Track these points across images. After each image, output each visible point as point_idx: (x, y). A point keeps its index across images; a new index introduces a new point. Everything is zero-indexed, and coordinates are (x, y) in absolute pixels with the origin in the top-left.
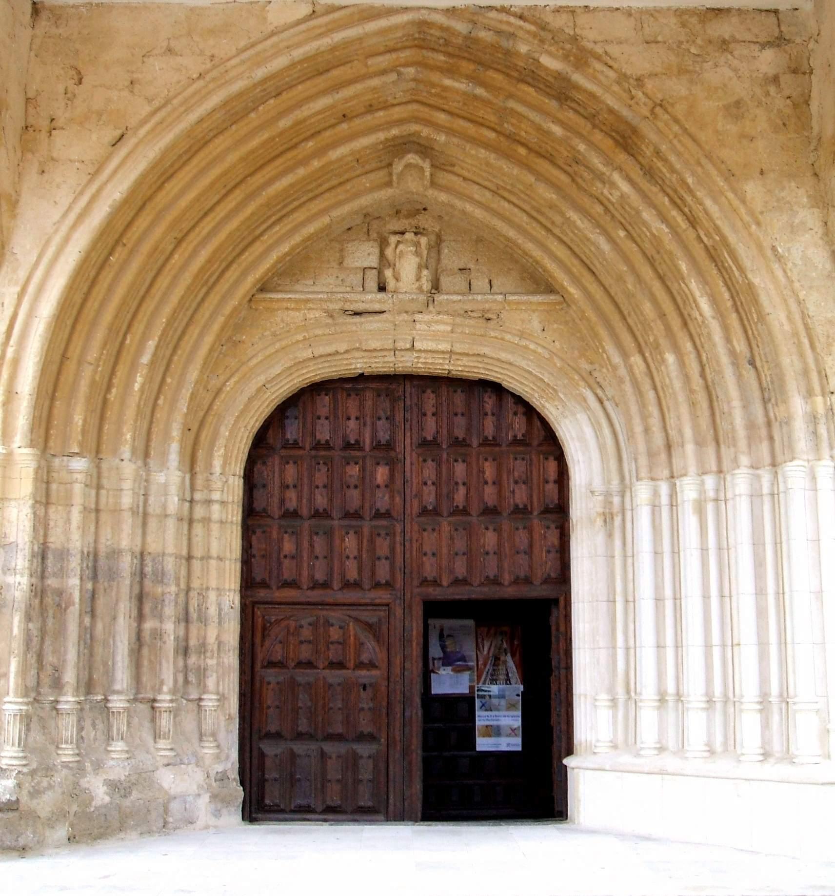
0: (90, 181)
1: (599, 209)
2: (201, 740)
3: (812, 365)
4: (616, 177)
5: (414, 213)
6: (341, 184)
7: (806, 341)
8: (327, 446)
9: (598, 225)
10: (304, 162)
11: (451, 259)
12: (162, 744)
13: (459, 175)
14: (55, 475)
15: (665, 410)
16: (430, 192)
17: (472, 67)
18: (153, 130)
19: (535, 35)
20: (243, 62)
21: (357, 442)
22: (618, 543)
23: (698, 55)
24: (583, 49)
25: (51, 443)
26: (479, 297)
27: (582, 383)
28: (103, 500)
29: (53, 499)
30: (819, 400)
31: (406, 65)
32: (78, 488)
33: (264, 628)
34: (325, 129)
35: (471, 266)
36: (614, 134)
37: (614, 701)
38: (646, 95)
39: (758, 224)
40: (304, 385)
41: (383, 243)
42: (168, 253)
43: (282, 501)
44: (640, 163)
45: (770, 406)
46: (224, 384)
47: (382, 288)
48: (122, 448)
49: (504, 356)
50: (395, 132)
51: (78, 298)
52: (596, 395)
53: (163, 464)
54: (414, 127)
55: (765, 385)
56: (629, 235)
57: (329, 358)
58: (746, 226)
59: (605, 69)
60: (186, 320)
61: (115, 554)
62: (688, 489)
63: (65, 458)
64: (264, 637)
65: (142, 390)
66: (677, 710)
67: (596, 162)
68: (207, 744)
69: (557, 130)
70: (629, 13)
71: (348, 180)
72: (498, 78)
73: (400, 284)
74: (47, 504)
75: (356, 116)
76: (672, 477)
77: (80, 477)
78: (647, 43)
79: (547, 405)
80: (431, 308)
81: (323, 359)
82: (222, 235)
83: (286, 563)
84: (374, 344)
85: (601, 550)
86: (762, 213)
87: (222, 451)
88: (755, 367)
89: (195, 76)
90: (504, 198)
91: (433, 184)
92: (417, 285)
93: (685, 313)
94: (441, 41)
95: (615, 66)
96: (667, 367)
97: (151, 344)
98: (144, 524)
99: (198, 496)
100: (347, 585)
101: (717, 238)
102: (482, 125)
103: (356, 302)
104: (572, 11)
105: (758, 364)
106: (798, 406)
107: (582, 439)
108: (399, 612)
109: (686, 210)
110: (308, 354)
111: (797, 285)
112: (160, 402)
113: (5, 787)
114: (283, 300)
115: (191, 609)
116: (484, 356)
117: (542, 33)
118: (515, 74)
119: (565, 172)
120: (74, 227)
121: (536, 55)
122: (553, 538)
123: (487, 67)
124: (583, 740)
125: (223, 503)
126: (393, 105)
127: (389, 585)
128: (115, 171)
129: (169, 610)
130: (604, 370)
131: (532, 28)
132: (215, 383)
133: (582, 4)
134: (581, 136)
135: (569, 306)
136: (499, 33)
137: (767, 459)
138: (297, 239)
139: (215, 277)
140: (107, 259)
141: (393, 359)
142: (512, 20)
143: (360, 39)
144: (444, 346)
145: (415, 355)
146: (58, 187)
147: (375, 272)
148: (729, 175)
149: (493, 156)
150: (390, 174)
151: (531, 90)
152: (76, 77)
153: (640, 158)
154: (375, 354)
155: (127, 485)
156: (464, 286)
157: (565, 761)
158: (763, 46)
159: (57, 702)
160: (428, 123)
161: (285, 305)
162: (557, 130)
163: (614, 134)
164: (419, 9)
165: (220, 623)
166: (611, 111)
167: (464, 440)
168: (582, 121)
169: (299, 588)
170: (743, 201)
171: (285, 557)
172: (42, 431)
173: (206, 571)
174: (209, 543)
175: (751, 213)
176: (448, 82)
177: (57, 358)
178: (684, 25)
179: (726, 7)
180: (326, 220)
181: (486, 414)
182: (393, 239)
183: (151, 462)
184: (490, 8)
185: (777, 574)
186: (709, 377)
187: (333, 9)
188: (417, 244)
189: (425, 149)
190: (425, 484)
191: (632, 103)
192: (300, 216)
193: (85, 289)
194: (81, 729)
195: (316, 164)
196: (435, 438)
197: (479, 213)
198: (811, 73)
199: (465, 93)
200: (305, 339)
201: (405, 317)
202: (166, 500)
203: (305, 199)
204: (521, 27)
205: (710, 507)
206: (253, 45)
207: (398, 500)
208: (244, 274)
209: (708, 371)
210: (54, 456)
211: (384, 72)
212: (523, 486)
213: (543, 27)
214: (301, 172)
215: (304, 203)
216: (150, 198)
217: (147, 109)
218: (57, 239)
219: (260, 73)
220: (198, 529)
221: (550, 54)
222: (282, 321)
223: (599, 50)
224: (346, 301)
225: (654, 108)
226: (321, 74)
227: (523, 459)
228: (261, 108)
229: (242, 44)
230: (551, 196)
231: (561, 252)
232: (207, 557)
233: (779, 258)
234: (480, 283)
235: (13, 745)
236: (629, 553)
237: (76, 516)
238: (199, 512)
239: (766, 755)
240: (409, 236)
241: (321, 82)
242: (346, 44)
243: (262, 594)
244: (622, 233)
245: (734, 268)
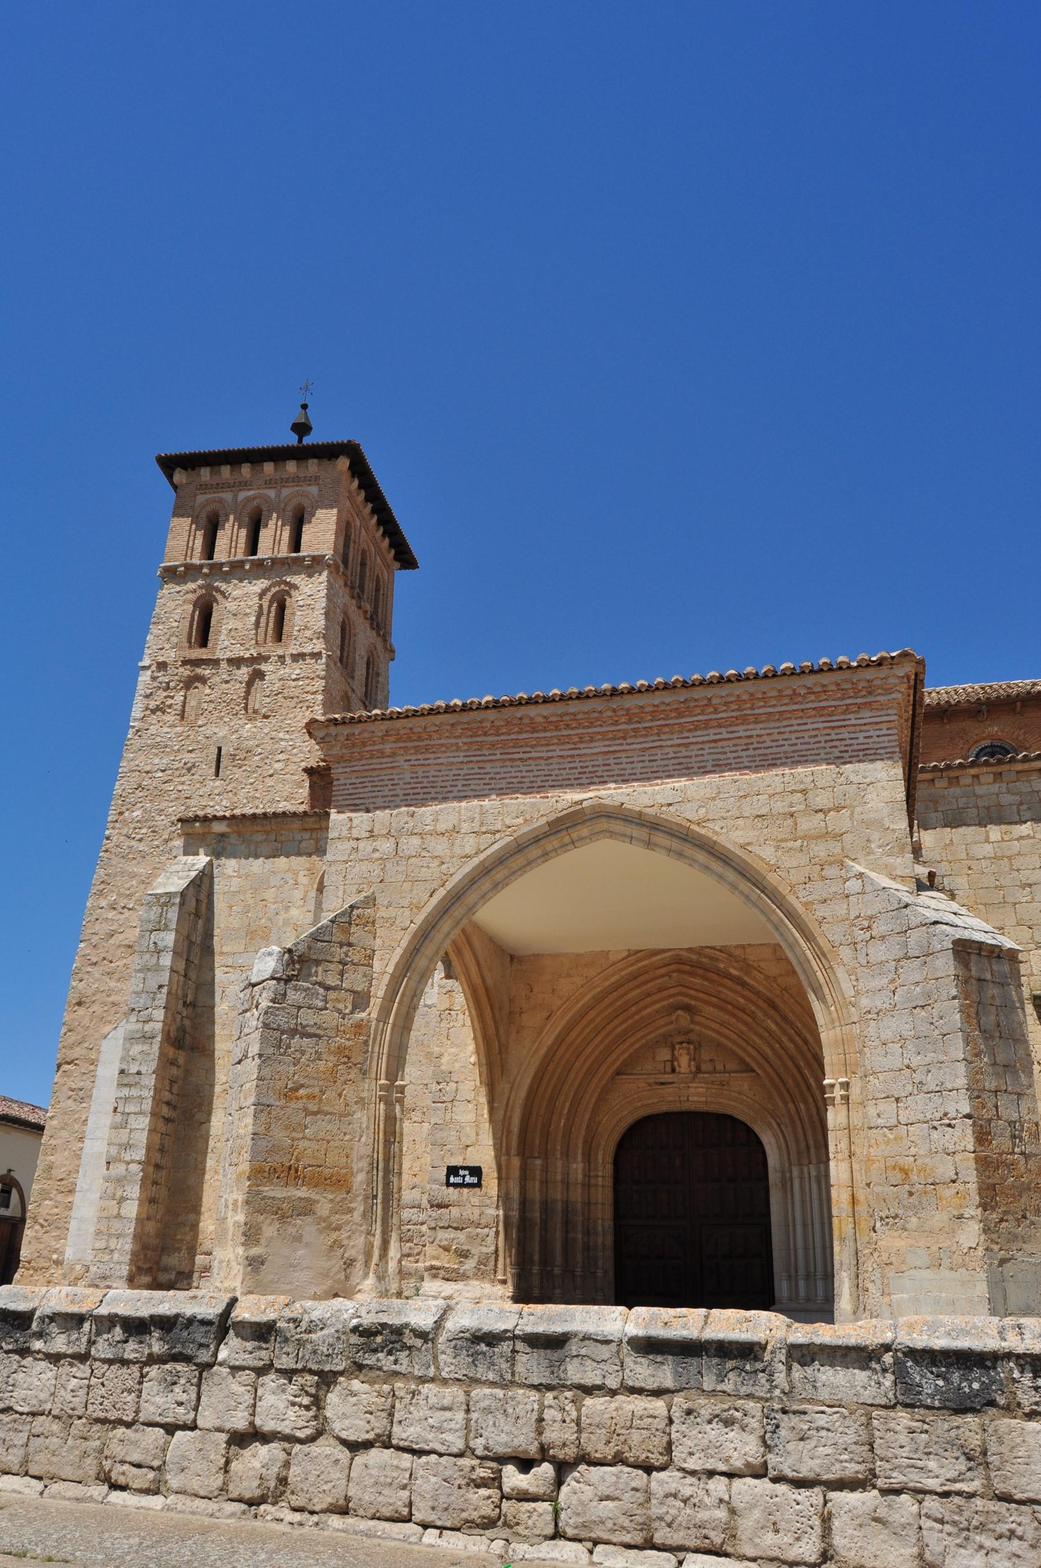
10: (631, 1017)
12: (578, 1292)
24: (749, 965)
31: (673, 972)
32: (538, 1172)
37: (790, 1276)
41: (673, 1049)
50: (671, 1000)
74: (525, 1180)
91: (692, 1021)
98: (568, 1188)
99: (592, 1174)
104: (743, 947)
125: (603, 1177)
129: (579, 1229)
144: (703, 1099)
168: (752, 995)
184: (707, 947)
188: (688, 1049)
192: (632, 1040)
194: (542, 1282)
195: (636, 1017)
214: (630, 1022)
217: (560, 1002)
219: (607, 983)
220: (593, 1189)
223: (755, 964)
229: (600, 970)
232: (596, 1203)
237: (537, 1184)
238: (593, 1181)
241: (635, 983)
242: (645, 966)
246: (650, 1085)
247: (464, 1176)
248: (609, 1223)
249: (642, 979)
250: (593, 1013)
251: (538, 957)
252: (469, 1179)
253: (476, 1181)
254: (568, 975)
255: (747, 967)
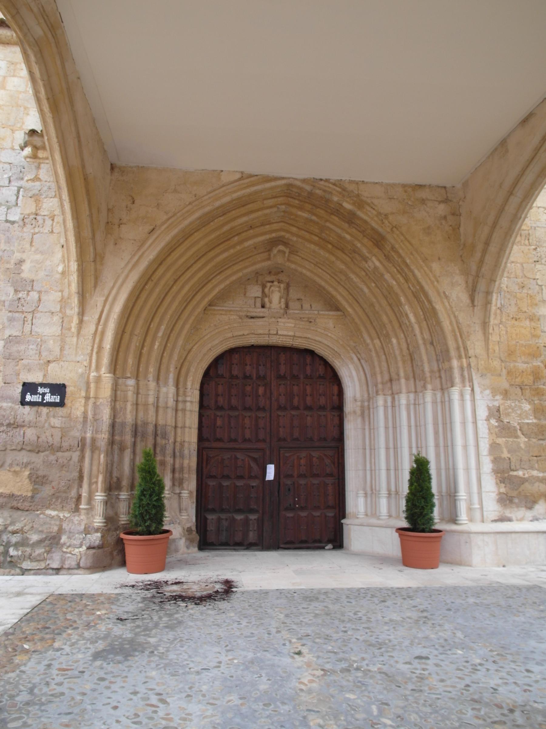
0: (139, 249)
1: (363, 273)
2: (180, 512)
3: (461, 345)
4: (374, 259)
5: (277, 274)
6: (247, 258)
7: (458, 334)
8: (237, 377)
9: (363, 281)
10: (233, 247)
11: (294, 294)
13: (300, 256)
14: (119, 387)
15: (390, 364)
16: (288, 264)
17: (310, 206)
18: (168, 227)
19: (340, 193)
20: (210, 198)
21: (250, 375)
22: (367, 423)
23: (412, 205)
25: (117, 372)
26: (307, 312)
27: (351, 352)
28: (140, 400)
29: (118, 398)
30: (464, 360)
33: (207, 460)
34: (243, 232)
35: (303, 298)
36: (372, 240)
37: (366, 494)
38: (389, 222)
39: (438, 281)
40: (227, 349)
41: (264, 286)
42: (171, 285)
43: (216, 402)
44: (383, 253)
45: (440, 363)
46: (192, 348)
47: (263, 307)
48: (149, 376)
49: (317, 338)
50: (274, 235)
51: (131, 305)
52: (357, 357)
53: (166, 384)
54: (283, 234)
55: (437, 353)
56: (377, 286)
57: (240, 337)
58: (432, 283)
59: (372, 210)
60: (177, 317)
61: (145, 424)
62: (403, 400)
63: (124, 379)
64: (207, 464)
65: (158, 348)
66: (396, 498)
67: (365, 251)
68: (183, 514)
69: (348, 237)
70: (381, 184)
71: (250, 257)
72: (322, 212)
73: (271, 305)
75: (257, 227)
76: (393, 394)
77: (131, 388)
78: (390, 199)
79: (335, 361)
80: (285, 316)
81: (237, 338)
82: (195, 279)
83: (218, 430)
84: (261, 332)
85: (360, 426)
86: (439, 277)
87: (191, 378)
88: (433, 345)
89: (187, 203)
90: (320, 268)
92: (279, 305)
93: (401, 321)
94: (297, 194)
95: (376, 208)
96: (392, 345)
97: (163, 327)
100: (245, 440)
101: (418, 287)
102: (312, 233)
103: (253, 312)
104: (357, 183)
105: (435, 344)
106: (455, 363)
107: (351, 377)
108: (268, 452)
109: (404, 274)
110: (230, 335)
111: (454, 309)
112: (165, 355)
113: (97, 536)
114: (220, 310)
115: (177, 451)
116: (309, 338)
117: (344, 192)
118: (329, 211)
119: (349, 257)
120: (131, 271)
121: (341, 202)
122: (336, 421)
123: (317, 207)
124: (352, 511)
125: (191, 402)
126: (273, 223)
127: (264, 441)
128: (152, 244)
130: (361, 346)
131: (340, 190)
132: (188, 347)
133: (362, 180)
134: (359, 240)
135: (346, 317)
136: (325, 191)
137: (439, 386)
138: (228, 282)
139: (190, 298)
140: (144, 287)
141: (268, 339)
142: (331, 185)
143: (262, 191)
144: (291, 333)
145: (278, 337)
146: (123, 251)
147: (260, 299)
148: (425, 260)
149: (317, 248)
150: (269, 255)
151: (336, 219)
152: (132, 201)
153: (384, 251)
154: (260, 336)
155: (151, 393)
156: (300, 306)
157: (343, 521)
158: (440, 202)
159: (119, 495)
160: (288, 232)
161: (221, 312)
162: (348, 237)
163: (372, 240)
164: (289, 178)
165: (190, 457)
166: (373, 229)
167: (297, 376)
169: (223, 441)
170: (431, 271)
171: (218, 427)
172: (113, 366)
173: (183, 433)
174: (185, 420)
175: (435, 276)
176: (300, 213)
177: (120, 332)
178: (406, 192)
179: (424, 184)
180: (240, 274)
181: (307, 364)
182: (269, 285)
183: (161, 383)
184: (321, 180)
185: (444, 438)
186: (411, 350)
187: (251, 176)
188: (279, 287)
189: (285, 243)
190: (280, 395)
191: (383, 225)
192: (229, 272)
193: (134, 301)
195: (238, 248)
196: (284, 375)
197: (308, 274)
198: (460, 215)
199: (307, 219)
200: (229, 328)
201: (273, 320)
202: (167, 400)
203: (231, 264)
204: (334, 189)
205: (412, 407)
206: (214, 190)
207: (268, 402)
208: (204, 297)
209: (410, 347)
210: (119, 378)
211: (271, 207)
212: (323, 397)
213: (344, 190)
214: (232, 251)
215: (231, 266)
216: (164, 260)
217: (165, 217)
218: (123, 275)
219: (217, 204)
220: (180, 414)
221: (347, 202)
222: (219, 319)
223: (369, 201)
224: (248, 311)
225: (392, 228)
226: (243, 206)
227: (323, 385)
228: (216, 221)
230: (343, 267)
231: (345, 293)
233: (447, 297)
234: (306, 306)
235: (100, 516)
236: (372, 428)
238: (180, 406)
239: (390, 516)
240: (276, 283)
241: (243, 210)
242: (256, 192)
243: (206, 444)
244: (373, 285)
245: (425, 301)
246: (241, 318)
247: (44, 395)
248: (194, 446)
249: (250, 207)
250: (197, 236)
251: (142, 169)
252: (48, 398)
253: (58, 400)
254: (175, 191)
255: (360, 203)
